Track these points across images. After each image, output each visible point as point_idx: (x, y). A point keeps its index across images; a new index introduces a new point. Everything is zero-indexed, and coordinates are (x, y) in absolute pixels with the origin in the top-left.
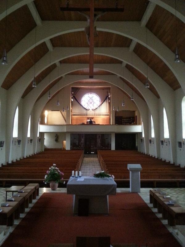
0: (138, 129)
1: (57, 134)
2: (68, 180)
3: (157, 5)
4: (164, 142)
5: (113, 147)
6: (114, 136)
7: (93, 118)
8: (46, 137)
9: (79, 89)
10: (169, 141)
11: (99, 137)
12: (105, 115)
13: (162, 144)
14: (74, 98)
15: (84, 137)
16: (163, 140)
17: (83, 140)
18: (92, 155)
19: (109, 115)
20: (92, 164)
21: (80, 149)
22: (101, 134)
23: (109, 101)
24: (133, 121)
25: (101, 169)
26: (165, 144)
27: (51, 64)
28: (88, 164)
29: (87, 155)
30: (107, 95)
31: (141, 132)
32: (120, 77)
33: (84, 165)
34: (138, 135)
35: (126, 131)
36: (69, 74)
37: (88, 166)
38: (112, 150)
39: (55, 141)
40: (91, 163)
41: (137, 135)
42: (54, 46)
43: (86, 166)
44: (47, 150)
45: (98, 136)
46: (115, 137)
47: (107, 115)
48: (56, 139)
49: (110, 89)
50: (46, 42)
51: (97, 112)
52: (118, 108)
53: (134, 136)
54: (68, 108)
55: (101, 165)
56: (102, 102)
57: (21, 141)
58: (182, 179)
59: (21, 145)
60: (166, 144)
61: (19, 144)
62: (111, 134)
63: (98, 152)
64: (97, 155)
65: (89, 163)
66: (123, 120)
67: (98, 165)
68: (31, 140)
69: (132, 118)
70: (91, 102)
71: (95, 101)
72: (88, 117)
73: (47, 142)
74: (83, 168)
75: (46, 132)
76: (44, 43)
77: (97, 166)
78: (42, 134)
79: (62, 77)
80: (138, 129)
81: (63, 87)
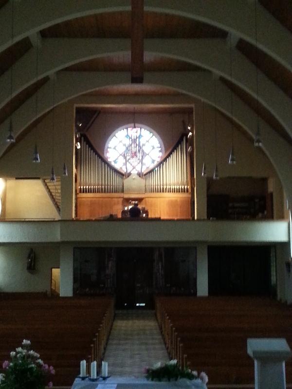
1: (32, 250)
5: (203, 288)
7: (140, 200)
9: (99, 114)
12: (178, 191)
17: (111, 267)
19: (190, 190)
25: (166, 354)
47: (183, 191)
51: (154, 181)
54: (65, 169)
69: (257, 200)
70: (135, 150)
71: (146, 149)
72: (126, 196)
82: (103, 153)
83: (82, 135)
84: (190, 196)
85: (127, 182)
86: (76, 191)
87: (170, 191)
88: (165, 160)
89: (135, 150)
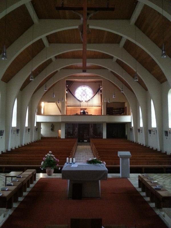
0: (128, 119)
1: (52, 124)
2: (63, 166)
3: (145, 4)
4: (151, 131)
5: (105, 136)
6: (106, 125)
7: (86, 109)
8: (42, 126)
10: (156, 131)
11: (92, 126)
12: (97, 106)
13: (150, 133)
14: (69, 90)
15: (78, 127)
16: (151, 130)
17: (77, 129)
18: (85, 143)
19: (101, 106)
20: (85, 152)
21: (74, 138)
22: (93, 124)
23: (101, 93)
24: (123, 111)
25: (93, 156)
26: (152, 133)
27: (47, 59)
28: (81, 151)
29: (81, 143)
30: (99, 88)
31: (130, 121)
32: (111, 71)
33: (78, 152)
34: (127, 125)
35: (116, 121)
36: (63, 68)
37: (81, 154)
38: (103, 138)
39: (51, 131)
40: (84, 151)
41: (126, 124)
42: (50, 42)
43: (79, 154)
44: (43, 138)
45: (91, 126)
46: (107, 126)
47: (99, 106)
48: (52, 128)
49: (102, 82)
50: (42, 39)
51: (90, 103)
52: (109, 100)
53: (124, 125)
54: (62, 99)
55: (93, 153)
56: (94, 95)
57: (20, 130)
58: (168, 166)
59: (19, 134)
60: (153, 133)
61: (17, 133)
62: (102, 124)
63: (91, 140)
64: (89, 143)
65: (82, 151)
66: (113, 111)
67: (90, 152)
68: (29, 130)
69: (122, 109)
70: (84, 94)
71: (88, 93)
73: (44, 131)
74: (77, 155)
75: (42, 122)
76: (41, 40)
77: (90, 153)
78: (39, 124)
79: (57, 71)
80: (128, 119)
81: (58, 80)
82: (74, 94)
83: (68, 89)
84: (101, 108)
85: (82, 104)
86: (66, 106)
87: (95, 106)
88: (93, 97)
89: (84, 94)
